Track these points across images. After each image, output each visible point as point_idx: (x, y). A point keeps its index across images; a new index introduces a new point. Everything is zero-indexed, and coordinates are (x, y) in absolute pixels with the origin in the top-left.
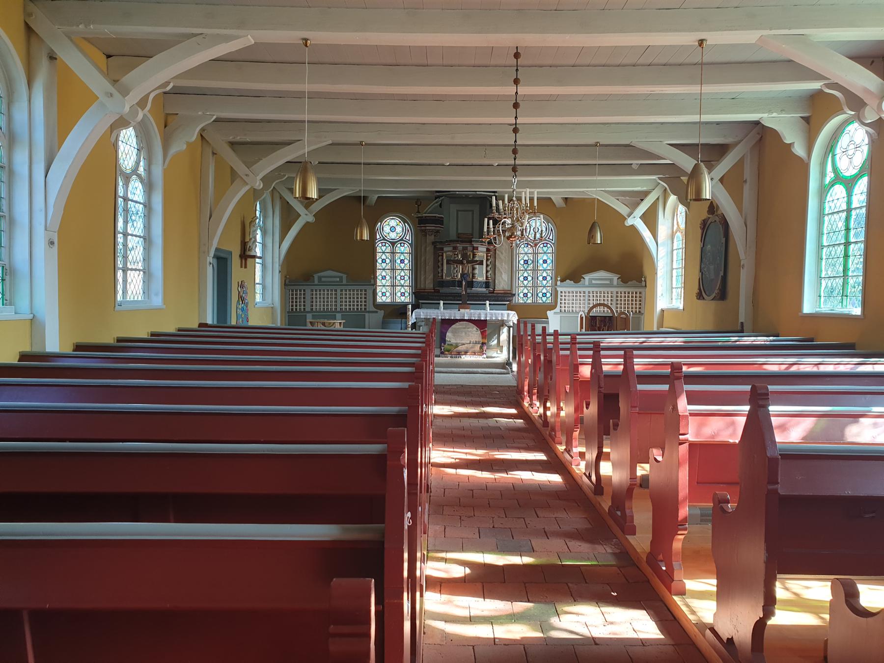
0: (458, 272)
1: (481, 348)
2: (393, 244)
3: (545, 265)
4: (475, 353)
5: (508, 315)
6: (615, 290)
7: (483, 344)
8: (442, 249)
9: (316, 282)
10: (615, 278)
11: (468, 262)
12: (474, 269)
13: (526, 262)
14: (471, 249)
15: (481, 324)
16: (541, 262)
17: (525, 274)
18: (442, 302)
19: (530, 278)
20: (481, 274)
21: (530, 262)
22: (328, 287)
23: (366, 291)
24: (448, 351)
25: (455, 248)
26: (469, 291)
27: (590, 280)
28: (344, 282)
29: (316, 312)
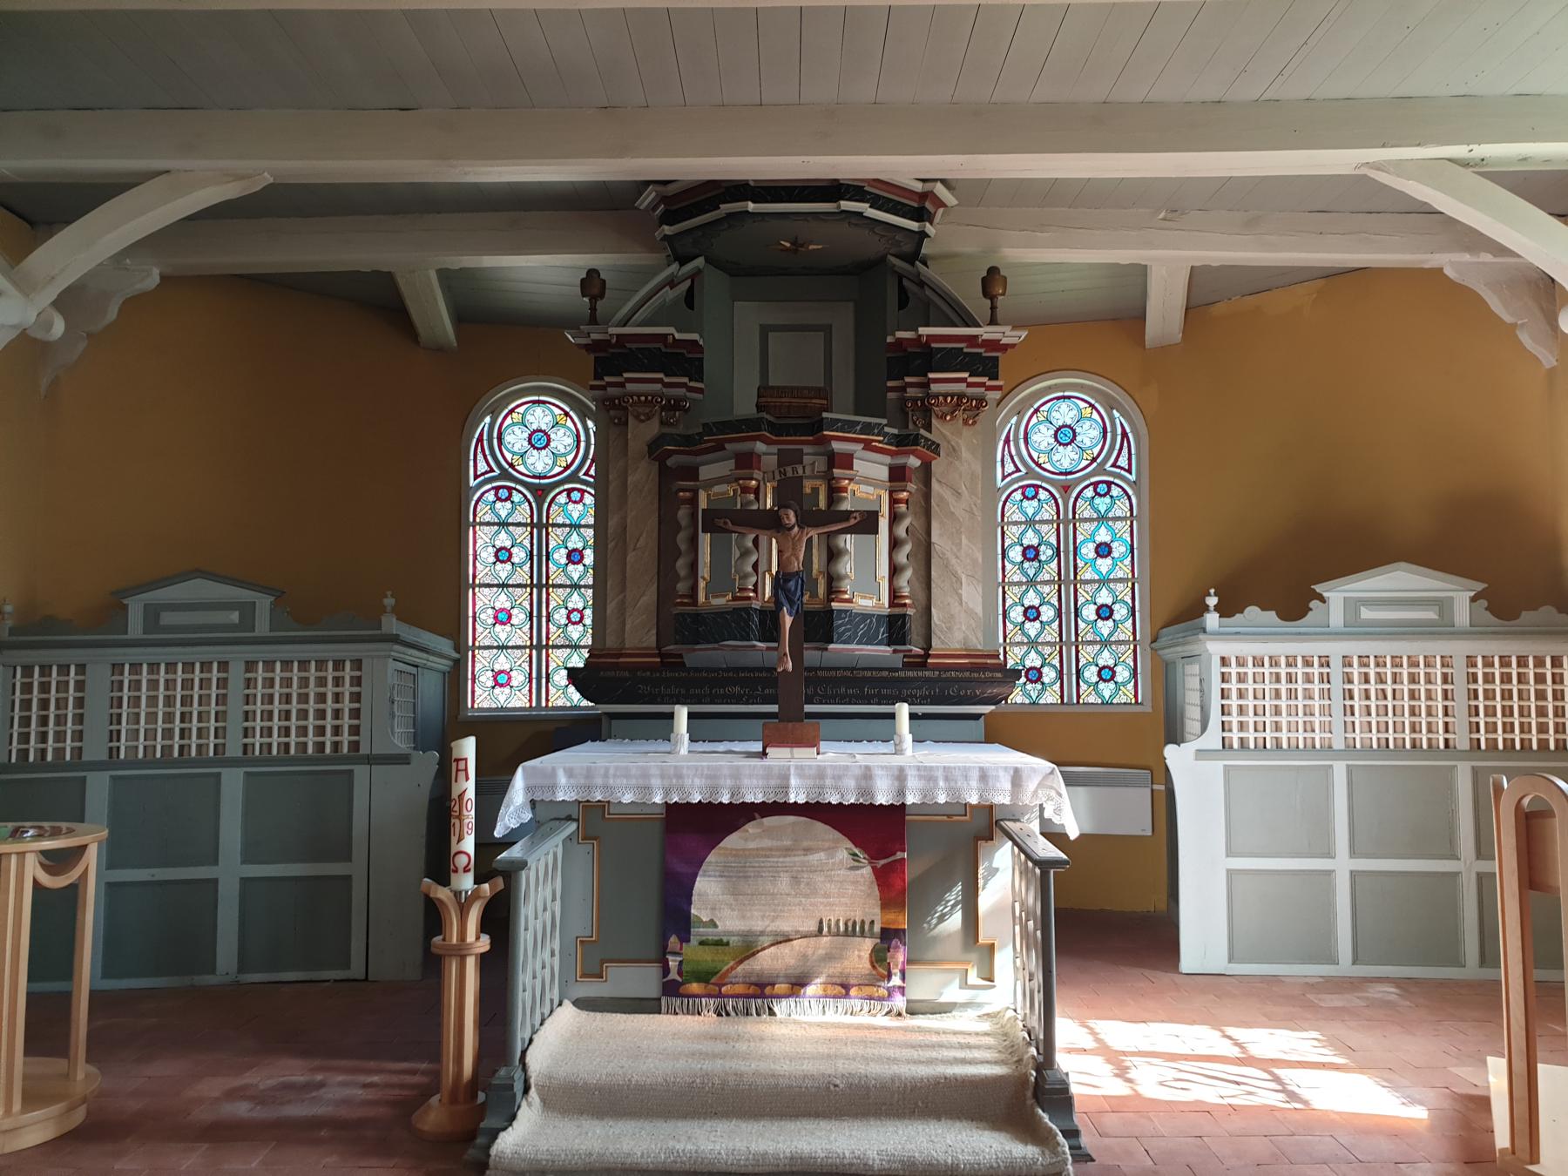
0: (767, 560)
1: (879, 958)
2: (540, 491)
3: (1104, 564)
4: (843, 988)
5: (1017, 777)
6: (1459, 649)
7: (889, 936)
8: (692, 473)
9: (135, 628)
10: (1460, 596)
11: (807, 520)
12: (833, 555)
13: (1031, 553)
14: (821, 464)
15: (874, 829)
16: (1088, 551)
17: (1032, 599)
18: (903, 710)
19: (1047, 613)
20: (866, 579)
21: (1046, 553)
22: (198, 654)
23: (357, 664)
24: (704, 976)
25: (747, 461)
26: (811, 656)
27: (1352, 606)
28: (262, 627)
29: (132, 763)
